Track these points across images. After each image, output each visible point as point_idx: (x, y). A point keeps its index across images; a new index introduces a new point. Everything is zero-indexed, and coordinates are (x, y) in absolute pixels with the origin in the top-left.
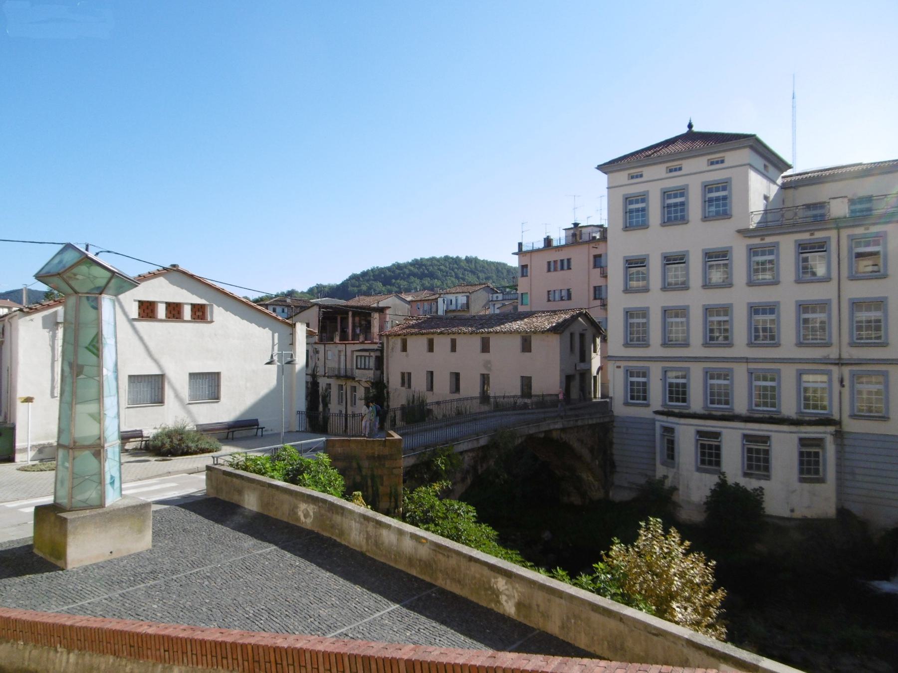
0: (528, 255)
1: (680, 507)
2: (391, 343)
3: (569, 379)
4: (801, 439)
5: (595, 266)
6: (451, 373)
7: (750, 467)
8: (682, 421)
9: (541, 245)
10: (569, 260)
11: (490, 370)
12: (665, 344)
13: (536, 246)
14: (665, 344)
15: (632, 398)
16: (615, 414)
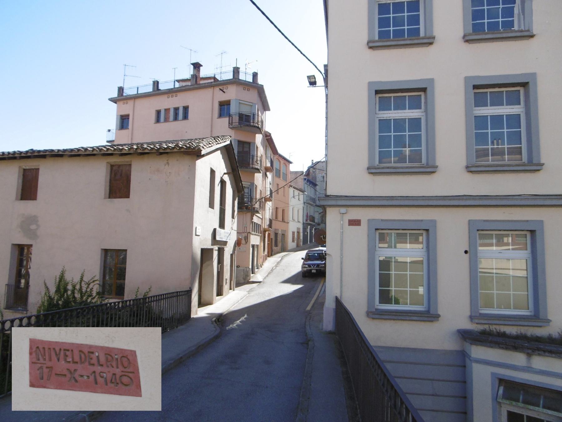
0: (131, 103)
4: (502, 381)
5: (221, 115)
6: (14, 245)
10: (186, 109)
11: (34, 235)
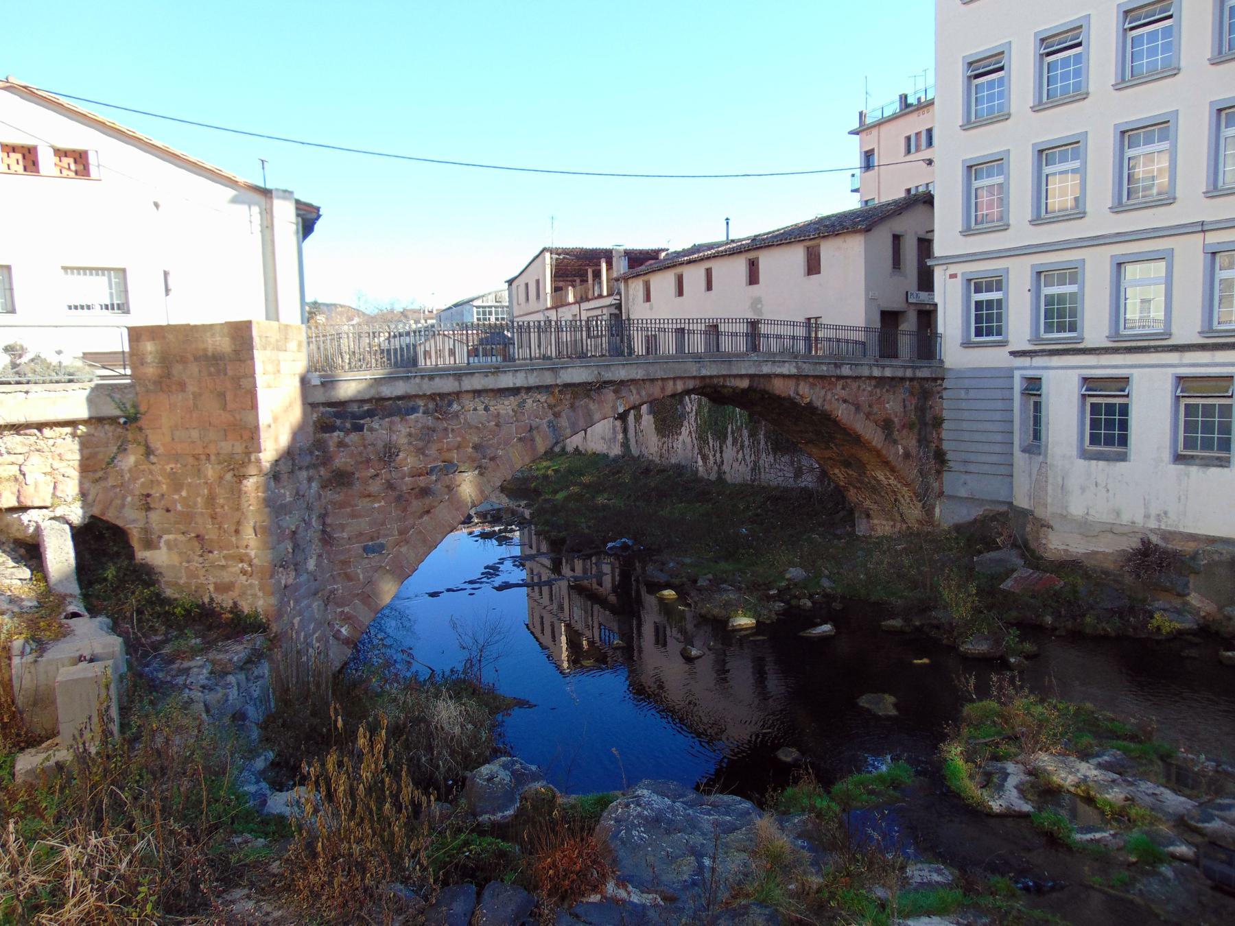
1: (1049, 527)
2: (631, 292)
3: (890, 318)
7: (1189, 443)
8: (1056, 361)
9: (895, 107)
12: (1038, 220)
13: (888, 113)
14: (1038, 220)
15: (979, 333)
16: (947, 365)
